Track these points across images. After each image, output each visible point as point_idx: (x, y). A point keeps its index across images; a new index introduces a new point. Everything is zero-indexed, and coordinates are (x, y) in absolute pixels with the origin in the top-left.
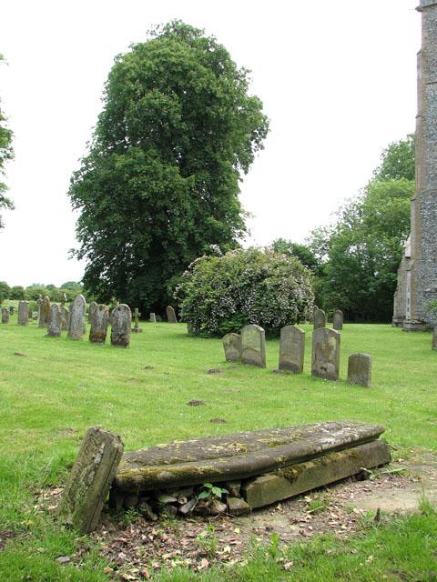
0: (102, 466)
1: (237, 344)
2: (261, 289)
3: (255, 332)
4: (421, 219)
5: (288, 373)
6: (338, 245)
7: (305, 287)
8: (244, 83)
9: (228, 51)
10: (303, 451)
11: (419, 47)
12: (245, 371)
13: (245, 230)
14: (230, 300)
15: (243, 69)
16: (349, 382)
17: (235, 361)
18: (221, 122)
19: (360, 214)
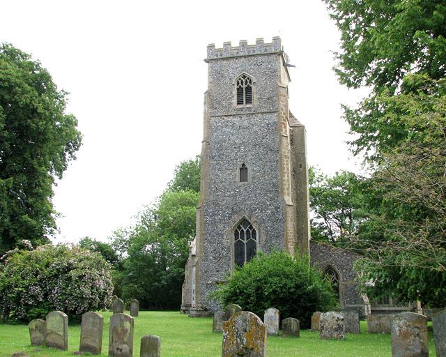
1: (41, 329)
3: (58, 318)
4: (204, 224)
6: (136, 243)
8: (62, 103)
11: (206, 89)
13: (55, 228)
14: (38, 289)
15: (63, 91)
17: (39, 344)
18: (40, 133)
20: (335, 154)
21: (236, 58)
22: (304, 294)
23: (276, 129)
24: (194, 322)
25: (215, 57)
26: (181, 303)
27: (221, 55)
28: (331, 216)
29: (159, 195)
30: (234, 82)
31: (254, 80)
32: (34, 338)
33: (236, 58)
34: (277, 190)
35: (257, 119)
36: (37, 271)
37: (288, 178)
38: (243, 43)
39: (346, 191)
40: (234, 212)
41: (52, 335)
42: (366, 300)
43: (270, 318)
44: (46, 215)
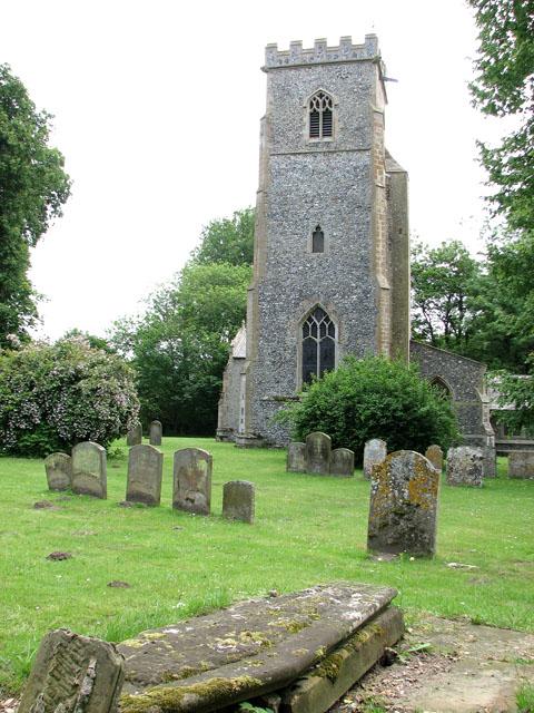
0: (96, 699)
1: (66, 468)
2: (73, 393)
3: (92, 452)
4: (260, 313)
5: (140, 507)
6: (147, 339)
7: (127, 396)
8: (43, 130)
9: (25, 86)
10: (338, 635)
11: (263, 113)
12: (78, 503)
13: (36, 316)
14: (34, 407)
15: (44, 112)
16: (225, 516)
17: (62, 489)
18: (11, 176)
19: (174, 303)
20: (455, 215)
21: (310, 66)
22: (414, 419)
23: (366, 174)
24: (250, 456)
25: (278, 65)
26: (216, 427)
27: (287, 61)
28: (431, 305)
29: (180, 270)
30: (306, 103)
31: (336, 100)
32: (53, 481)
33: (310, 66)
34: (367, 264)
35: (338, 160)
36: (32, 382)
37: (382, 248)
38: (321, 44)
39: (456, 269)
40: (302, 297)
41: (83, 477)
42: (489, 428)
43: (373, 453)
44: (22, 298)
